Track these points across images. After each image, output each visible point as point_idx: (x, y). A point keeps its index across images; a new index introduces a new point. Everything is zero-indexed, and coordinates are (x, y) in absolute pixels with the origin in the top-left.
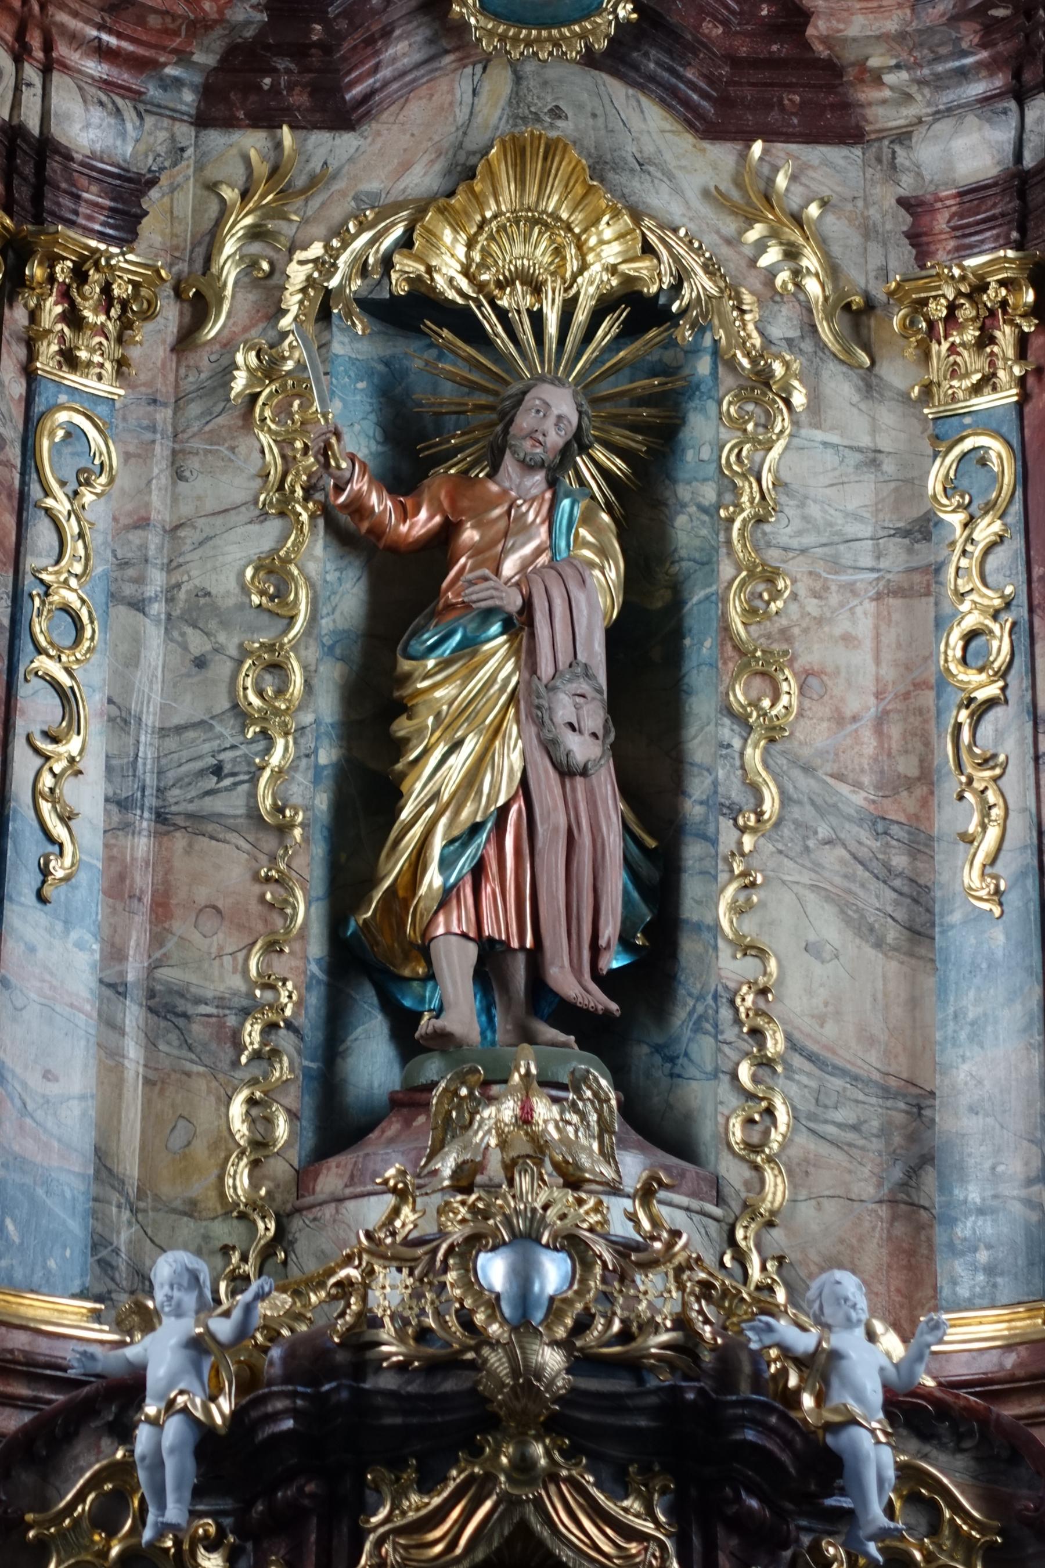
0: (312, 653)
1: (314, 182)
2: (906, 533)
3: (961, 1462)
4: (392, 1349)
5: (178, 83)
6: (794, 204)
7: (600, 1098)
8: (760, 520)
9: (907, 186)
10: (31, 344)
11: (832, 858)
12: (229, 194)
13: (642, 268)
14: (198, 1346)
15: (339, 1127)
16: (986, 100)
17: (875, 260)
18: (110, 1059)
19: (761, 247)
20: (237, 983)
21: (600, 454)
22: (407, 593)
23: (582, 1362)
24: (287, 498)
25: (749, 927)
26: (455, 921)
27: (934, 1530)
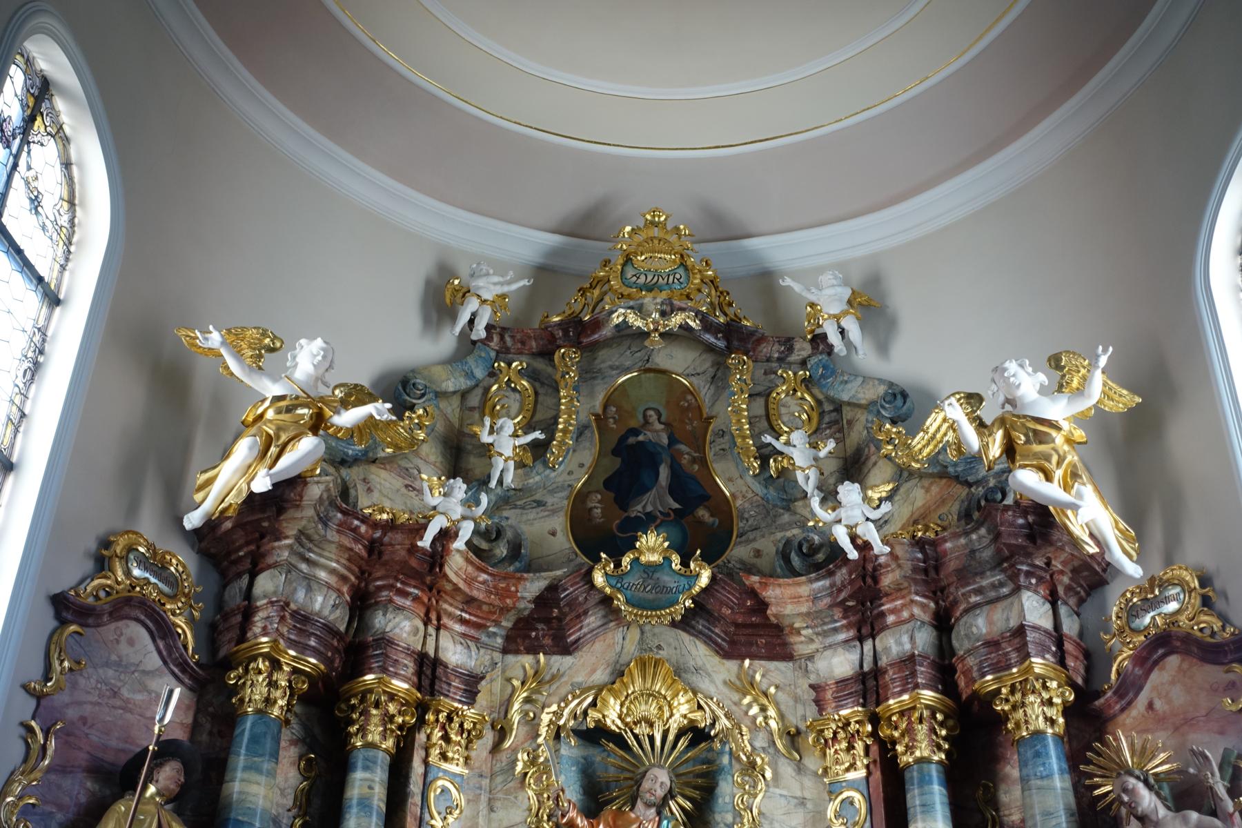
1: (554, 678)
5: (495, 634)
6: (764, 687)
9: (813, 679)
10: (427, 750)
12: (516, 683)
13: (697, 715)
16: (846, 641)
19: (750, 706)
21: (680, 800)
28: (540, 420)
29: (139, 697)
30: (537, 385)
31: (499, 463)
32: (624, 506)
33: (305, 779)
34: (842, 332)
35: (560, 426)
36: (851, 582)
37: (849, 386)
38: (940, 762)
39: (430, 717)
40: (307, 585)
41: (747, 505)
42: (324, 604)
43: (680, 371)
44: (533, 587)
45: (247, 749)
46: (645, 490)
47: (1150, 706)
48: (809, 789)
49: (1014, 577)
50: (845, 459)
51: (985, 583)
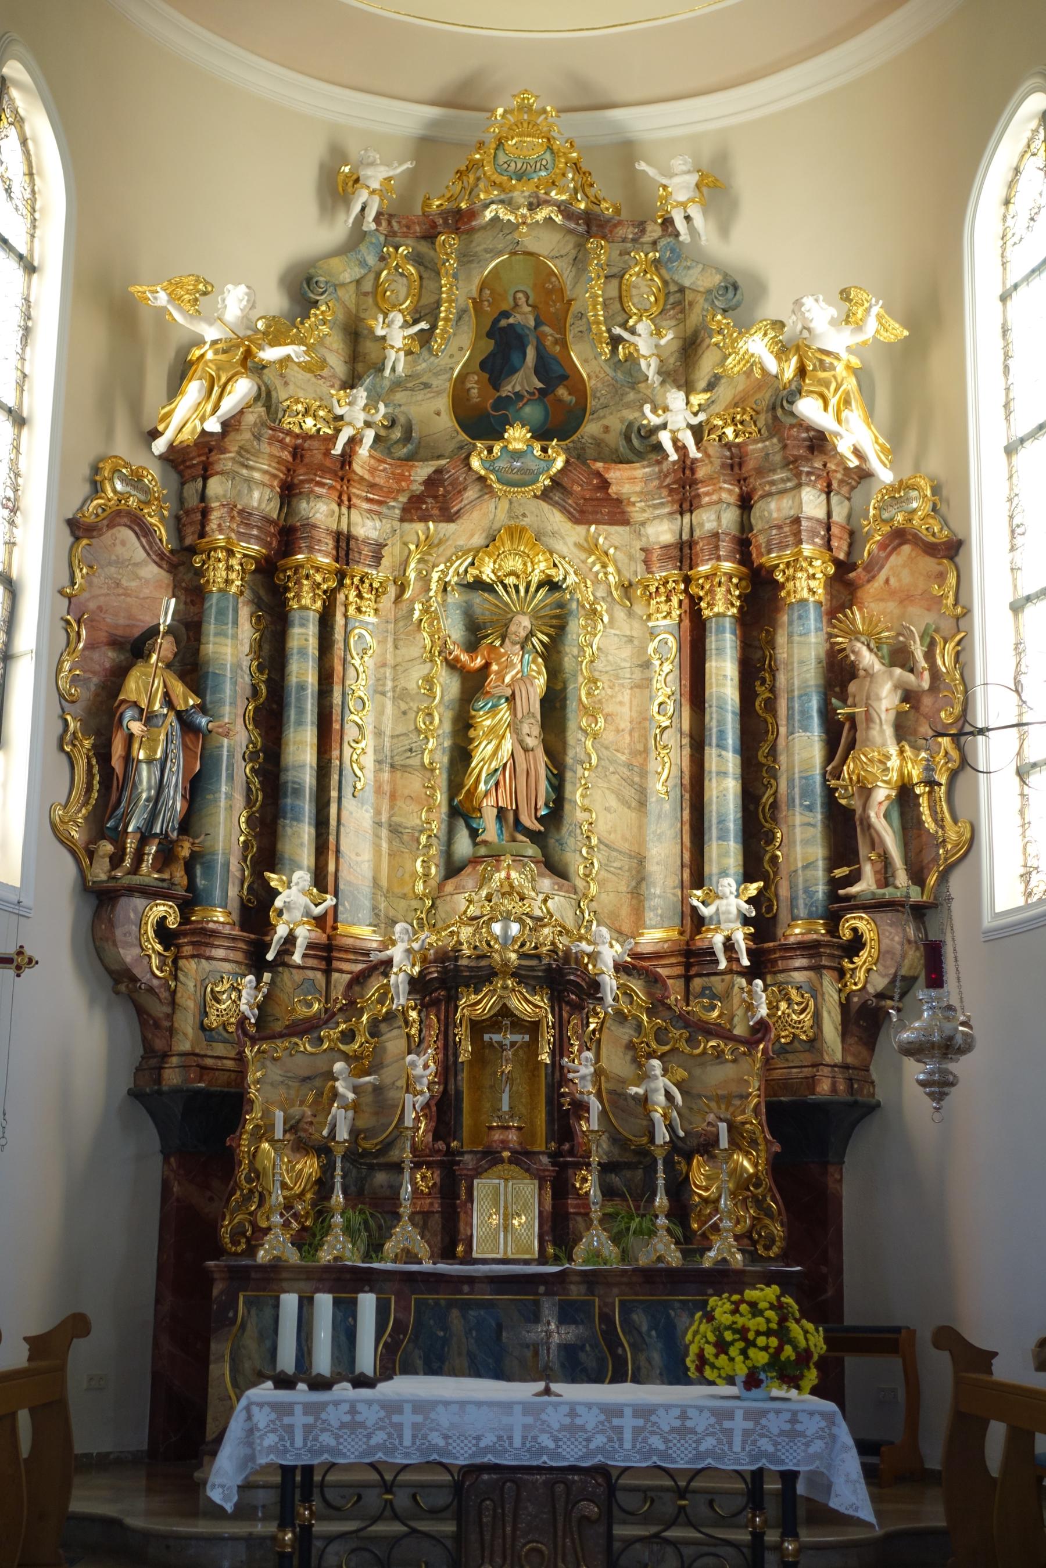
0: (441, 709)
1: (440, 543)
2: (641, 666)
3: (640, 982)
4: (467, 952)
5: (394, 507)
6: (606, 548)
7: (531, 870)
8: (592, 662)
9: (643, 543)
10: (346, 606)
11: (614, 778)
12: (412, 547)
13: (552, 572)
14: (409, 951)
15: (453, 869)
16: (671, 514)
17: (633, 569)
18: (377, 848)
19: (594, 564)
20: (418, 822)
21: (540, 635)
22: (473, 685)
23: (522, 956)
24: (433, 655)
25: (586, 802)
26: (490, 801)
27: (631, 1003)
28: (425, 312)
29: (133, 584)
30: (422, 268)
31: (392, 355)
32: (496, 387)
33: (257, 631)
34: (688, 218)
35: (442, 315)
36: (675, 471)
37: (691, 272)
38: (733, 616)
39: (347, 581)
40: (248, 489)
41: (599, 385)
42: (261, 499)
43: (546, 253)
44: (422, 471)
45: (216, 619)
46: (514, 371)
47: (887, 581)
48: (636, 629)
49: (798, 475)
50: (685, 339)
51: (776, 477)
